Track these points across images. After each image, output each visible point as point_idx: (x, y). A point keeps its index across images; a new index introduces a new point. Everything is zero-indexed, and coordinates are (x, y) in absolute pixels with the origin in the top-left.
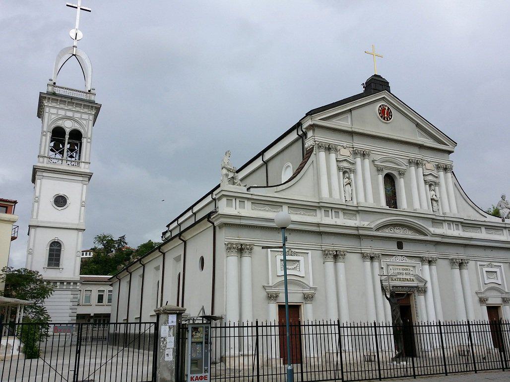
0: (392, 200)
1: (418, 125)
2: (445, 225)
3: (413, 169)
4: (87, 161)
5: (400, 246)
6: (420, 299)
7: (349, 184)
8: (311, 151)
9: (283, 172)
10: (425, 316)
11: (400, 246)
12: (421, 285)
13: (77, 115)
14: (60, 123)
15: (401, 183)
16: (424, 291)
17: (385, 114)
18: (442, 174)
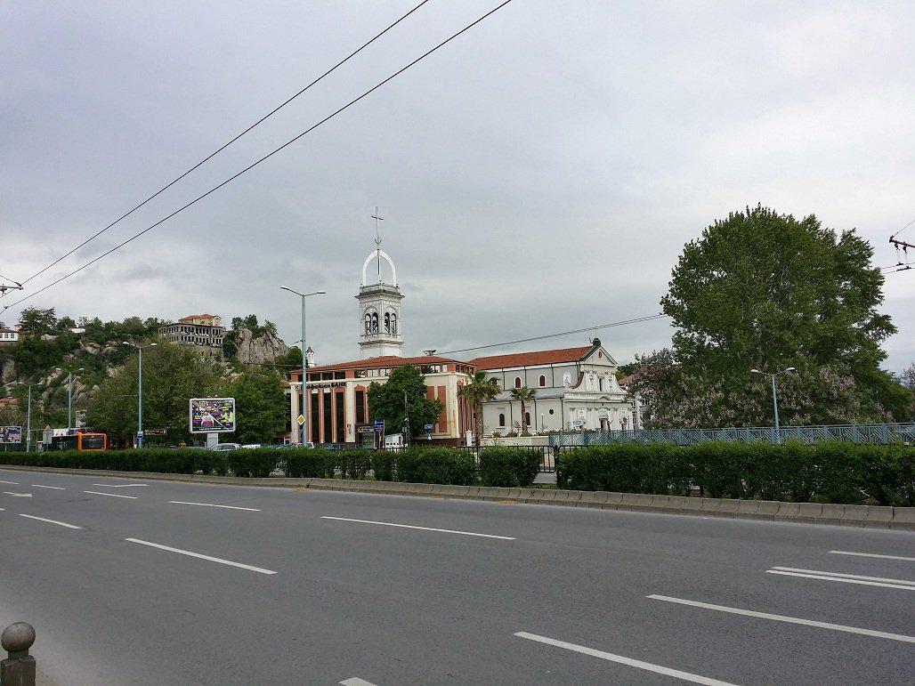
17: (600, 356)
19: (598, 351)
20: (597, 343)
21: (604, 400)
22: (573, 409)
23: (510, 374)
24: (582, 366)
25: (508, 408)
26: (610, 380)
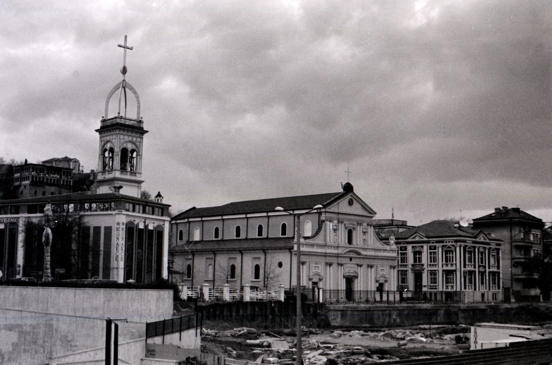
0: (350, 241)
1: (362, 206)
2: (368, 250)
3: (359, 227)
4: (140, 172)
5: (351, 260)
7: (336, 235)
8: (323, 221)
9: (305, 225)
10: (115, 167)
11: (351, 260)
12: (356, 275)
13: (135, 139)
14: (125, 145)
15: (354, 233)
17: (351, 203)
18: (369, 227)
19: (348, 197)
20: (348, 188)
21: (352, 255)
22: (371, 267)
23: (231, 222)
24: (323, 215)
25: (239, 257)
26: (364, 233)
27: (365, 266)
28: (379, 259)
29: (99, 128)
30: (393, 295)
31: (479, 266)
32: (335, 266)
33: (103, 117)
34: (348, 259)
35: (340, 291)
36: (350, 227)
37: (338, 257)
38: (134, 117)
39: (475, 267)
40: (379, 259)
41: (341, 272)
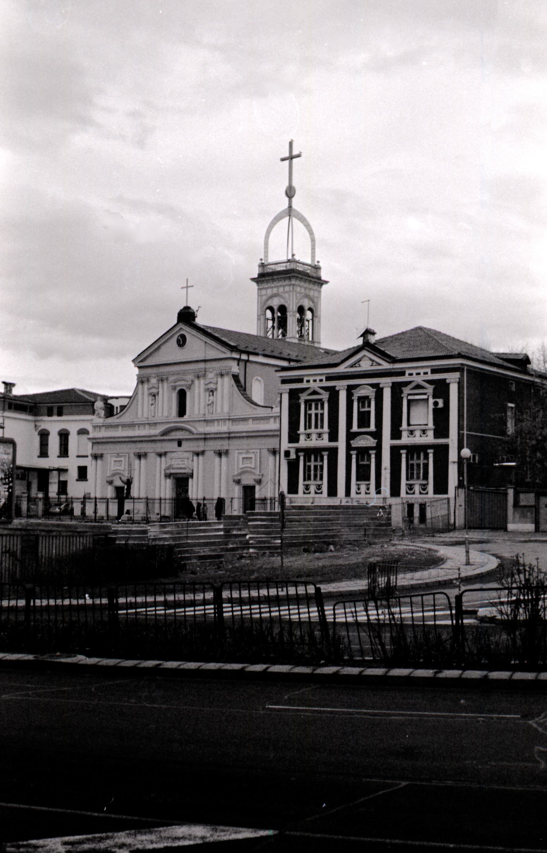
5: (180, 444)
6: (190, 480)
11: (180, 444)
16: (192, 476)
27: (210, 454)
28: (243, 437)
29: (256, 276)
30: (93, 505)
31: (351, 436)
32: (152, 457)
33: (261, 260)
34: (176, 444)
35: (163, 501)
36: (183, 385)
37: (205, 439)
38: (308, 260)
39: (334, 436)
40: (243, 437)
41: (161, 464)
